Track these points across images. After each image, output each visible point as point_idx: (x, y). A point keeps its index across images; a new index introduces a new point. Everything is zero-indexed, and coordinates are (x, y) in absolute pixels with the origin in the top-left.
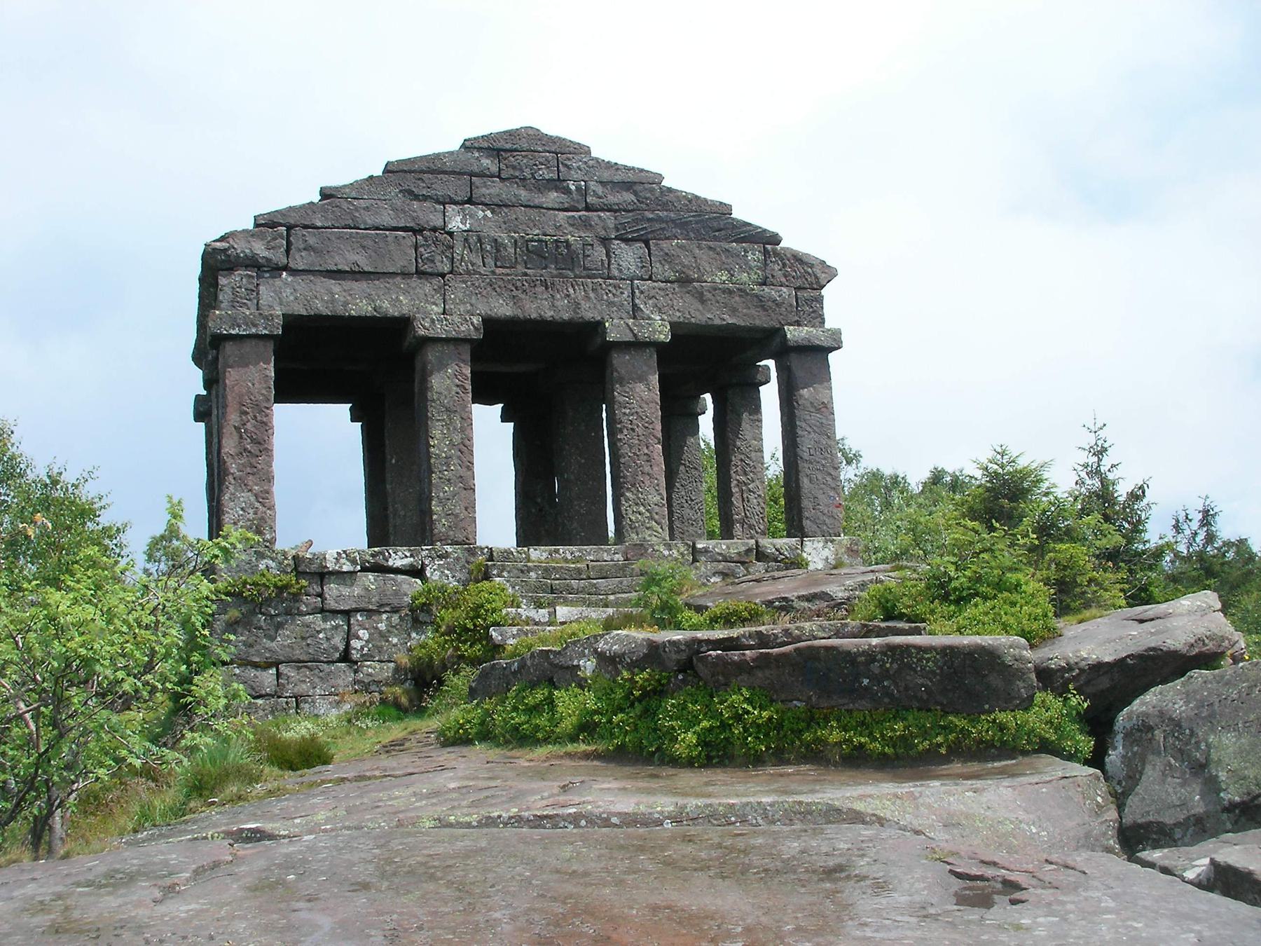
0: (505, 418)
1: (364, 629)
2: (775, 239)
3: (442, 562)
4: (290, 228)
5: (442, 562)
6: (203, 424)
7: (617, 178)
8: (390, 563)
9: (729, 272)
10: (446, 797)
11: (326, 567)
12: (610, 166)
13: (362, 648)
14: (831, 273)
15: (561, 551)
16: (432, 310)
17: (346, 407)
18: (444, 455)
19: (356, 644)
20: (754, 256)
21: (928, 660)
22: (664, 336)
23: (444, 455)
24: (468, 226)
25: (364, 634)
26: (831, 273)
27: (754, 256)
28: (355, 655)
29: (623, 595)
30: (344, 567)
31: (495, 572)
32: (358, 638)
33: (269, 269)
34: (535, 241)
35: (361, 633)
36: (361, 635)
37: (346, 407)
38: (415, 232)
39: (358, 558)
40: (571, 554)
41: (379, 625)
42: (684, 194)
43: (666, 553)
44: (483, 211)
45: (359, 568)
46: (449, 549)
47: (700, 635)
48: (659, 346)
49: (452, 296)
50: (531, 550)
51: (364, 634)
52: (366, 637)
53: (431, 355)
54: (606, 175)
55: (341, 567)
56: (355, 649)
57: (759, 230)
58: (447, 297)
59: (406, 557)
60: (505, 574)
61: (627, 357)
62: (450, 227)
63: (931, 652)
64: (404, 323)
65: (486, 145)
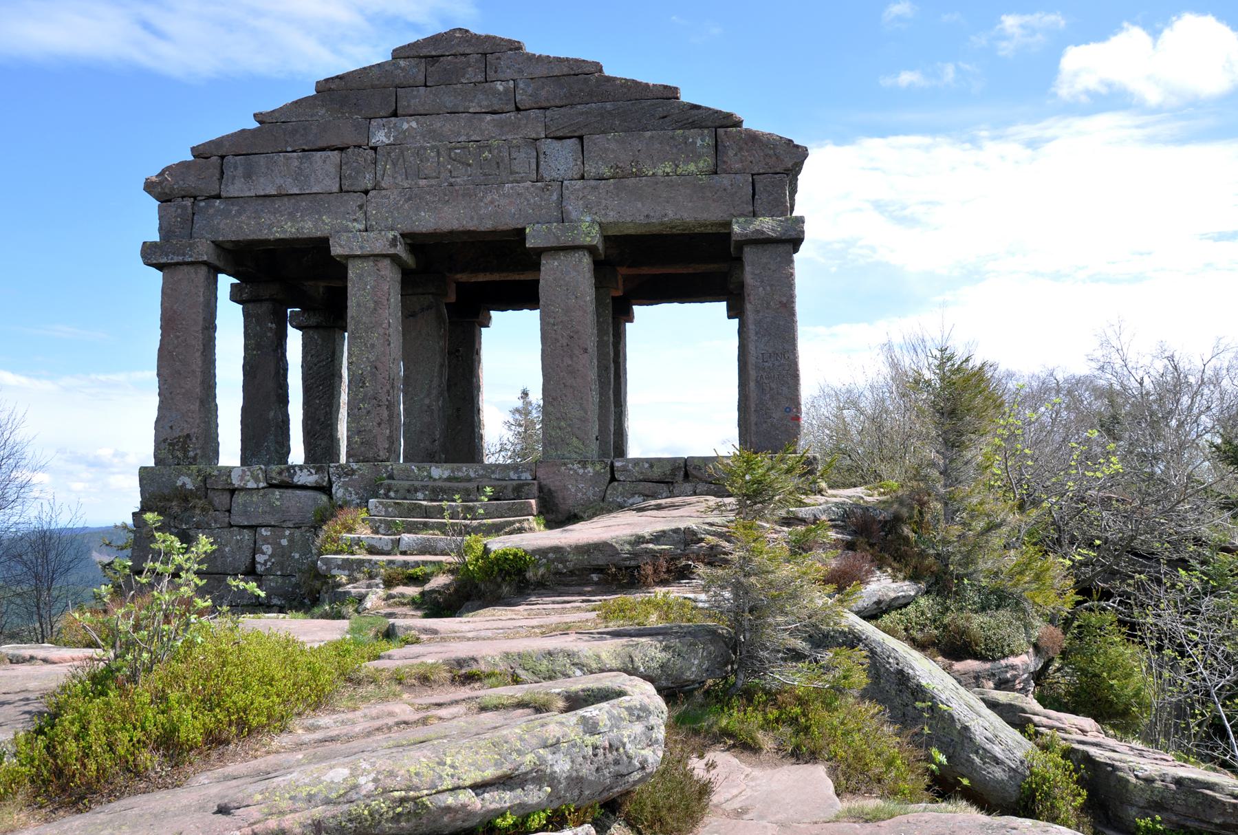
1: (268, 544)
2: (728, 122)
3: (347, 479)
4: (222, 157)
5: (347, 479)
6: (736, 321)
7: (565, 70)
8: (295, 480)
9: (674, 162)
10: (988, 665)
11: (231, 483)
12: (547, 60)
13: (266, 562)
16: (354, 227)
17: (724, 305)
19: (260, 558)
20: (702, 140)
22: (593, 237)
24: (392, 139)
25: (268, 549)
27: (702, 140)
28: (260, 569)
29: (490, 521)
30: (249, 484)
33: (203, 198)
34: (458, 148)
35: (264, 548)
36: (265, 550)
37: (724, 305)
38: (341, 149)
40: (475, 472)
41: (282, 541)
42: (623, 81)
43: (581, 471)
44: (408, 122)
48: (591, 250)
49: (374, 212)
50: (433, 468)
52: (270, 552)
53: (749, 254)
54: (541, 71)
55: (245, 484)
56: (259, 563)
57: (710, 112)
58: (369, 214)
60: (392, 494)
61: (556, 263)
62: (373, 141)
64: (322, 244)
65: (414, 53)
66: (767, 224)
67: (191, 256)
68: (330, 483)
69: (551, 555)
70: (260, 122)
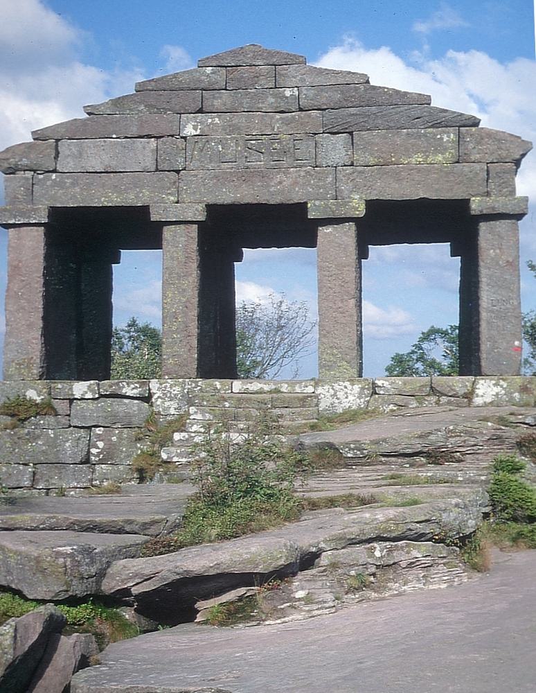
19: (94, 451)
64: (145, 210)
66: (497, 203)
67: (35, 219)
68: (150, 396)
69: (352, 446)
70: (89, 114)
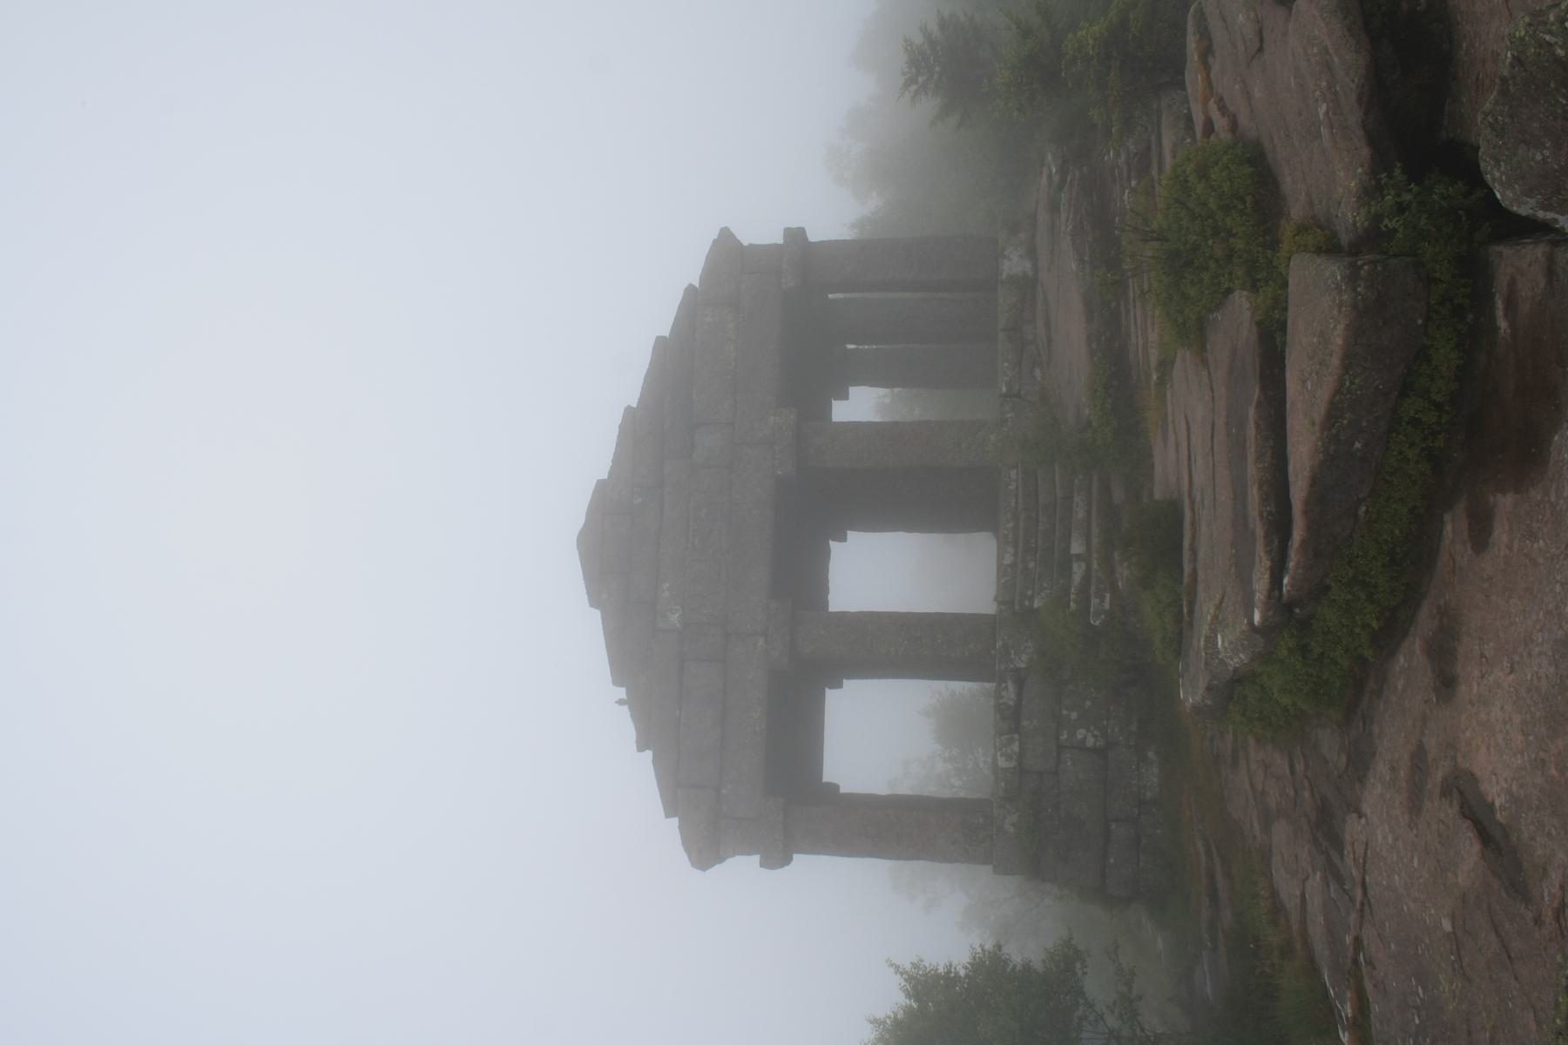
0: (843, 539)
3: (1012, 652)
5: (1012, 652)
8: (1011, 703)
14: (726, 237)
15: (1006, 532)
18: (906, 642)
19: (1090, 742)
21: (1352, 383)
23: (906, 642)
25: (1081, 733)
26: (726, 237)
28: (1101, 743)
31: (1027, 603)
32: (1085, 738)
39: (1007, 736)
45: (1016, 736)
46: (999, 644)
47: (1259, 596)
51: (1081, 733)
59: (1006, 687)
62: (678, 625)
63: (1345, 380)
